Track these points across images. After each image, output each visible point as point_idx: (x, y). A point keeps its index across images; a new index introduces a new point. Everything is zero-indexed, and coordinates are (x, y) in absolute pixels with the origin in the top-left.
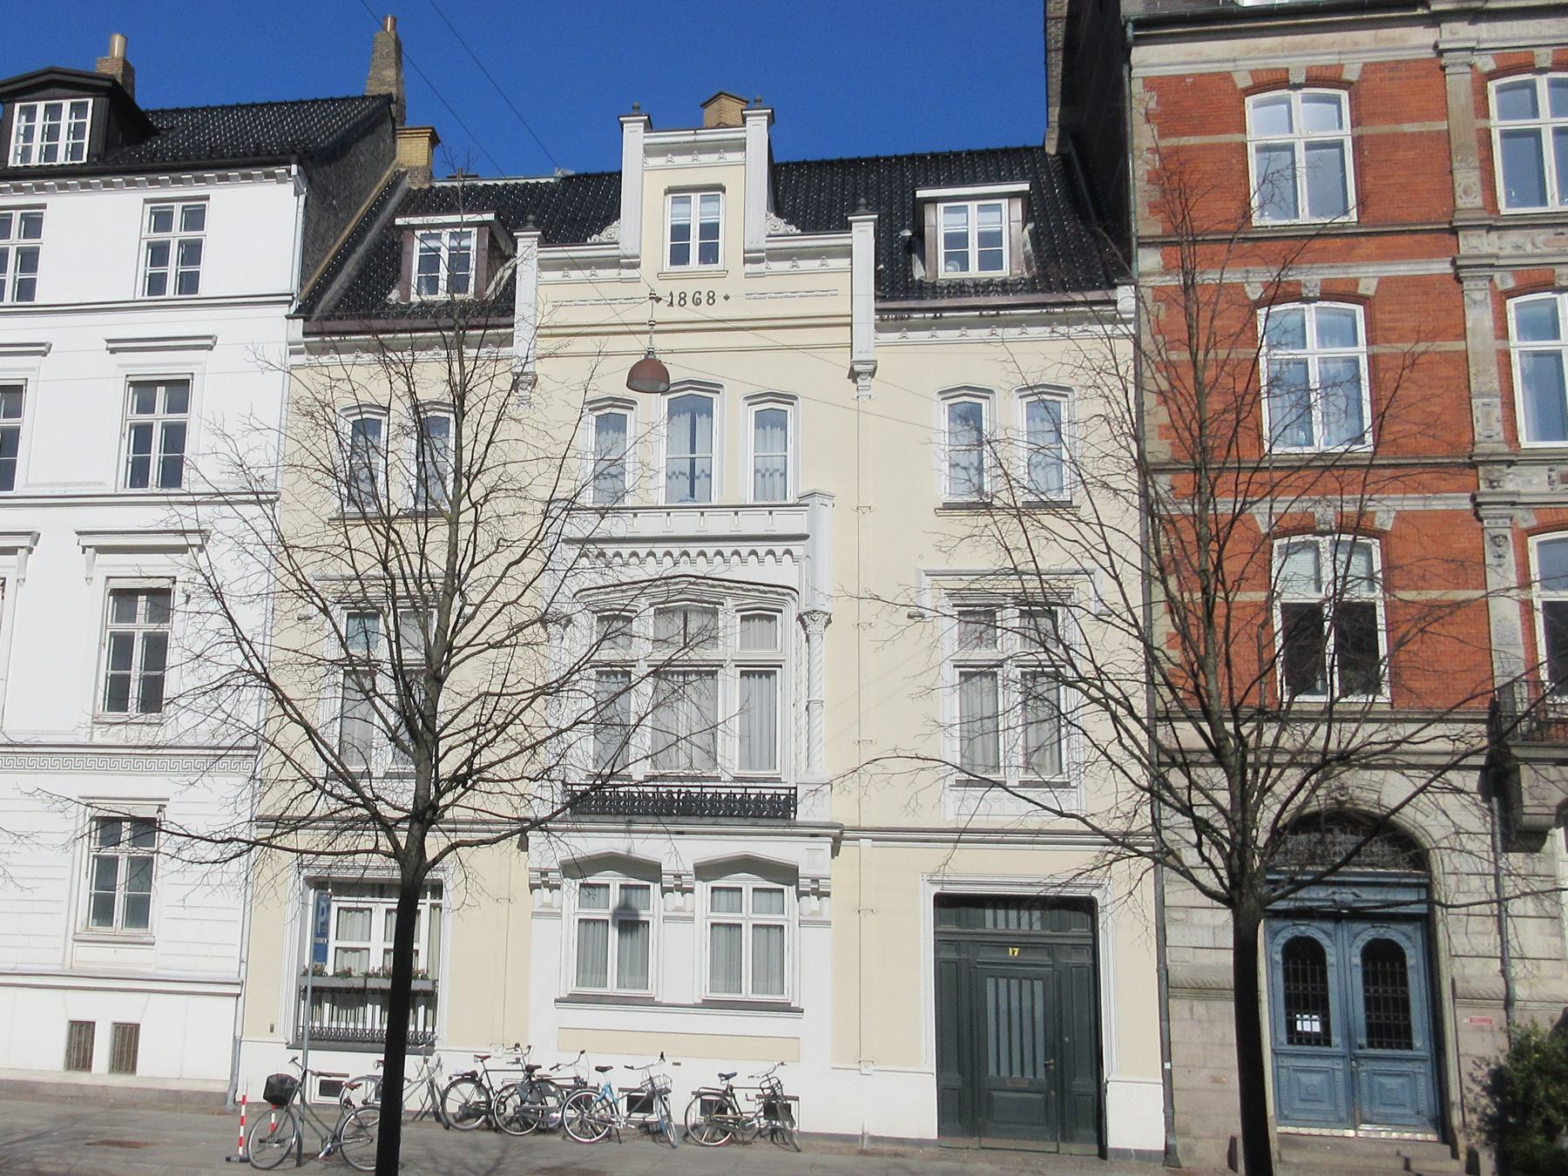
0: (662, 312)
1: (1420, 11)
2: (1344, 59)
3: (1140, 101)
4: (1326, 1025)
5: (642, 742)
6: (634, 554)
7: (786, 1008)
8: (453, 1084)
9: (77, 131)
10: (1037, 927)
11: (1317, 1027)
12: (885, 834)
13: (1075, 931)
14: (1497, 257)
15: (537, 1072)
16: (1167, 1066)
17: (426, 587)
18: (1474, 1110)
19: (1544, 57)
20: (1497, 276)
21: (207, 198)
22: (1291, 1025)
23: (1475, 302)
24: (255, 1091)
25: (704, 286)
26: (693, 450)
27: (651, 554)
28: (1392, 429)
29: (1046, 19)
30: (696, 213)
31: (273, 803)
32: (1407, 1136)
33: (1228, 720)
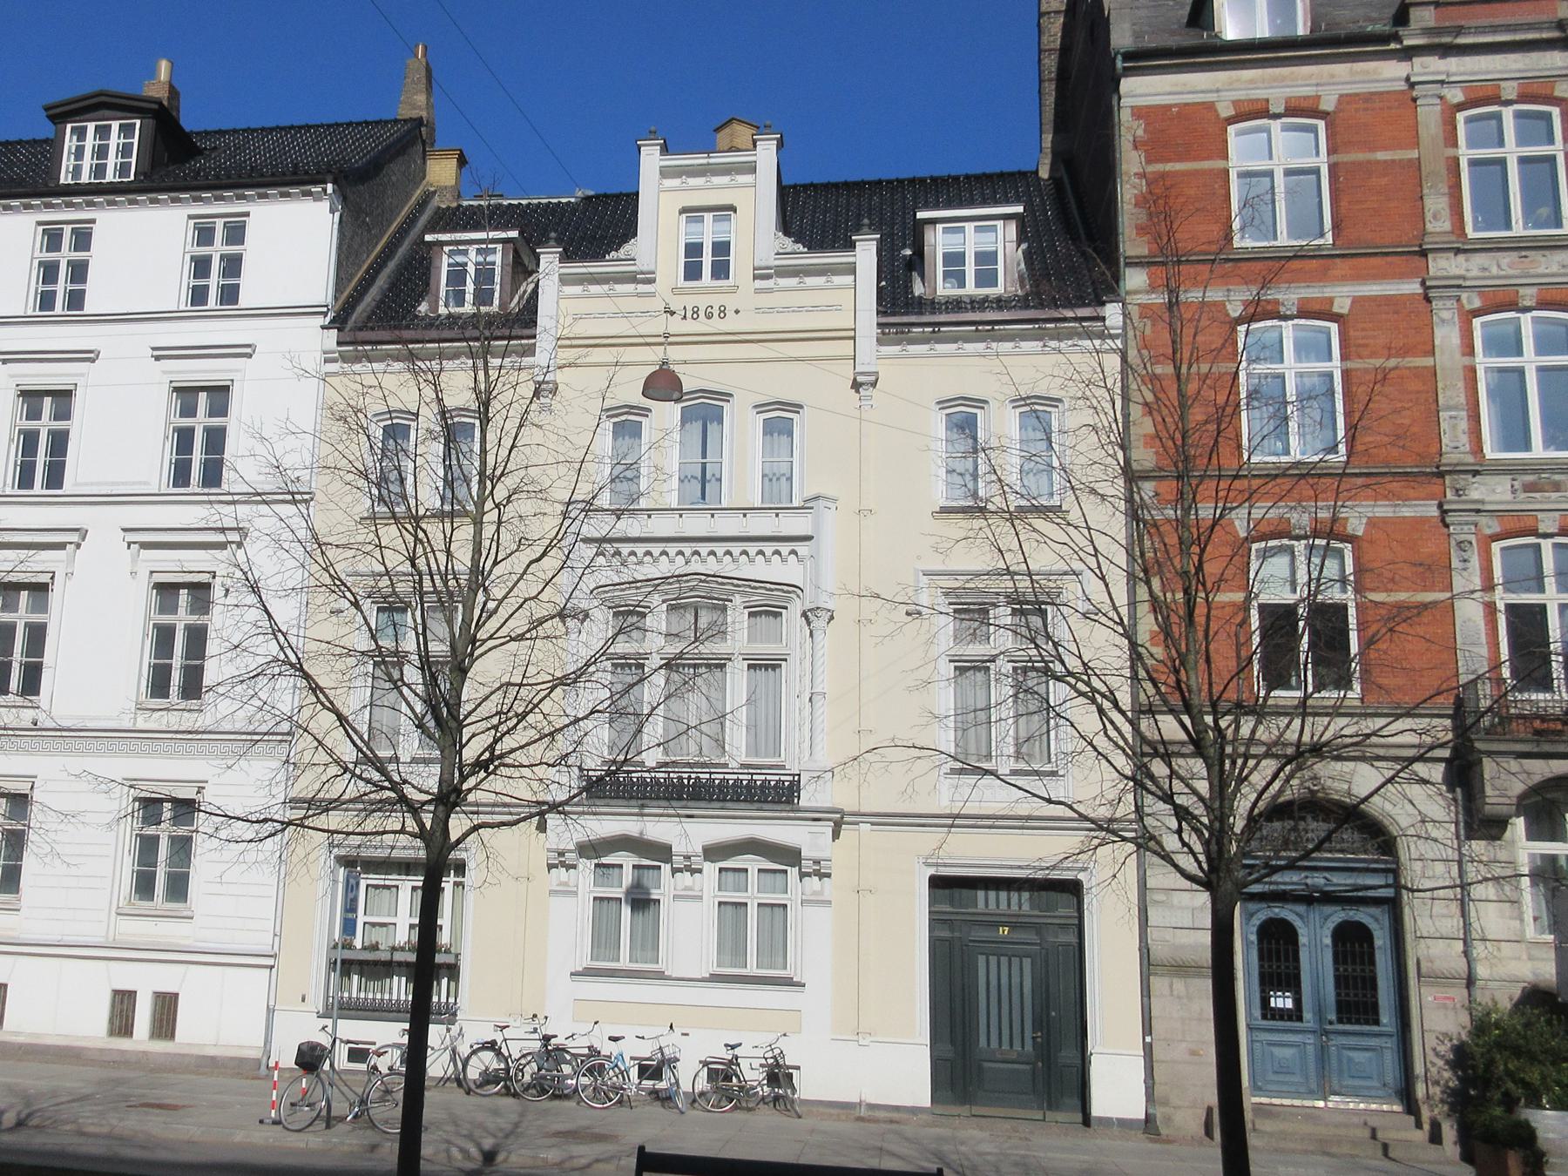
1: (1393, 46)
2: (1321, 91)
3: (1128, 129)
9: (125, 151)
10: (1026, 907)
12: (883, 819)
19: (1509, 90)
20: (1464, 296)
21: (247, 214)
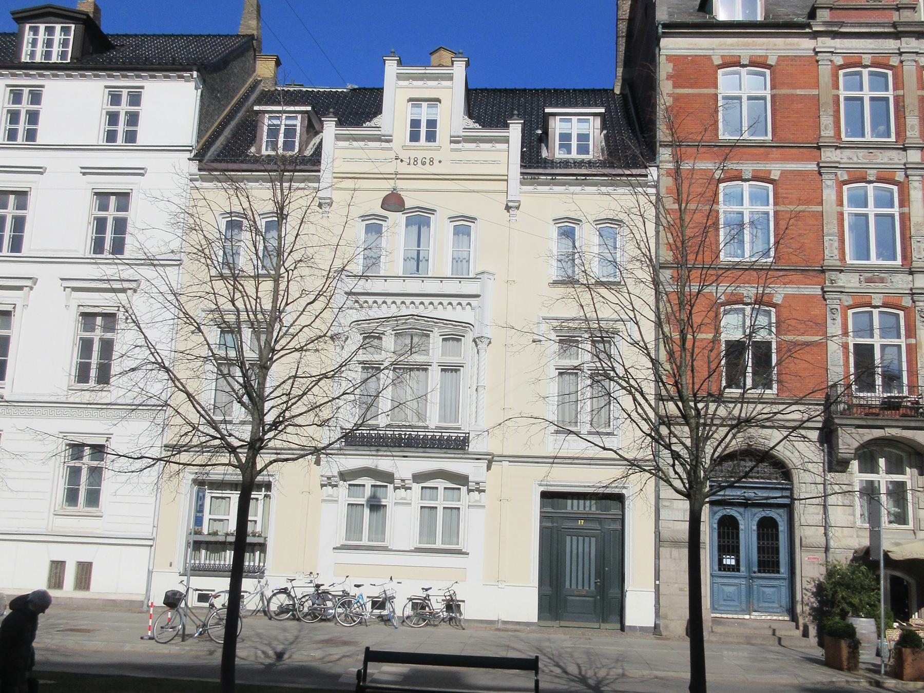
0: (403, 168)
1: (807, 30)
2: (769, 53)
3: (664, 69)
4: (738, 561)
5: (385, 404)
6: (375, 302)
7: (460, 552)
8: (274, 595)
9: (65, 43)
10: (593, 509)
11: (733, 562)
13: (613, 511)
14: (840, 163)
15: (322, 588)
16: (657, 582)
17: (260, 316)
18: (807, 604)
20: (839, 173)
22: (720, 561)
23: (828, 186)
24: (158, 600)
25: (428, 155)
26: (419, 246)
27: (384, 302)
28: (783, 249)
29: (617, 20)
30: (424, 113)
31: (170, 437)
32: (775, 618)
33: (691, 401)
